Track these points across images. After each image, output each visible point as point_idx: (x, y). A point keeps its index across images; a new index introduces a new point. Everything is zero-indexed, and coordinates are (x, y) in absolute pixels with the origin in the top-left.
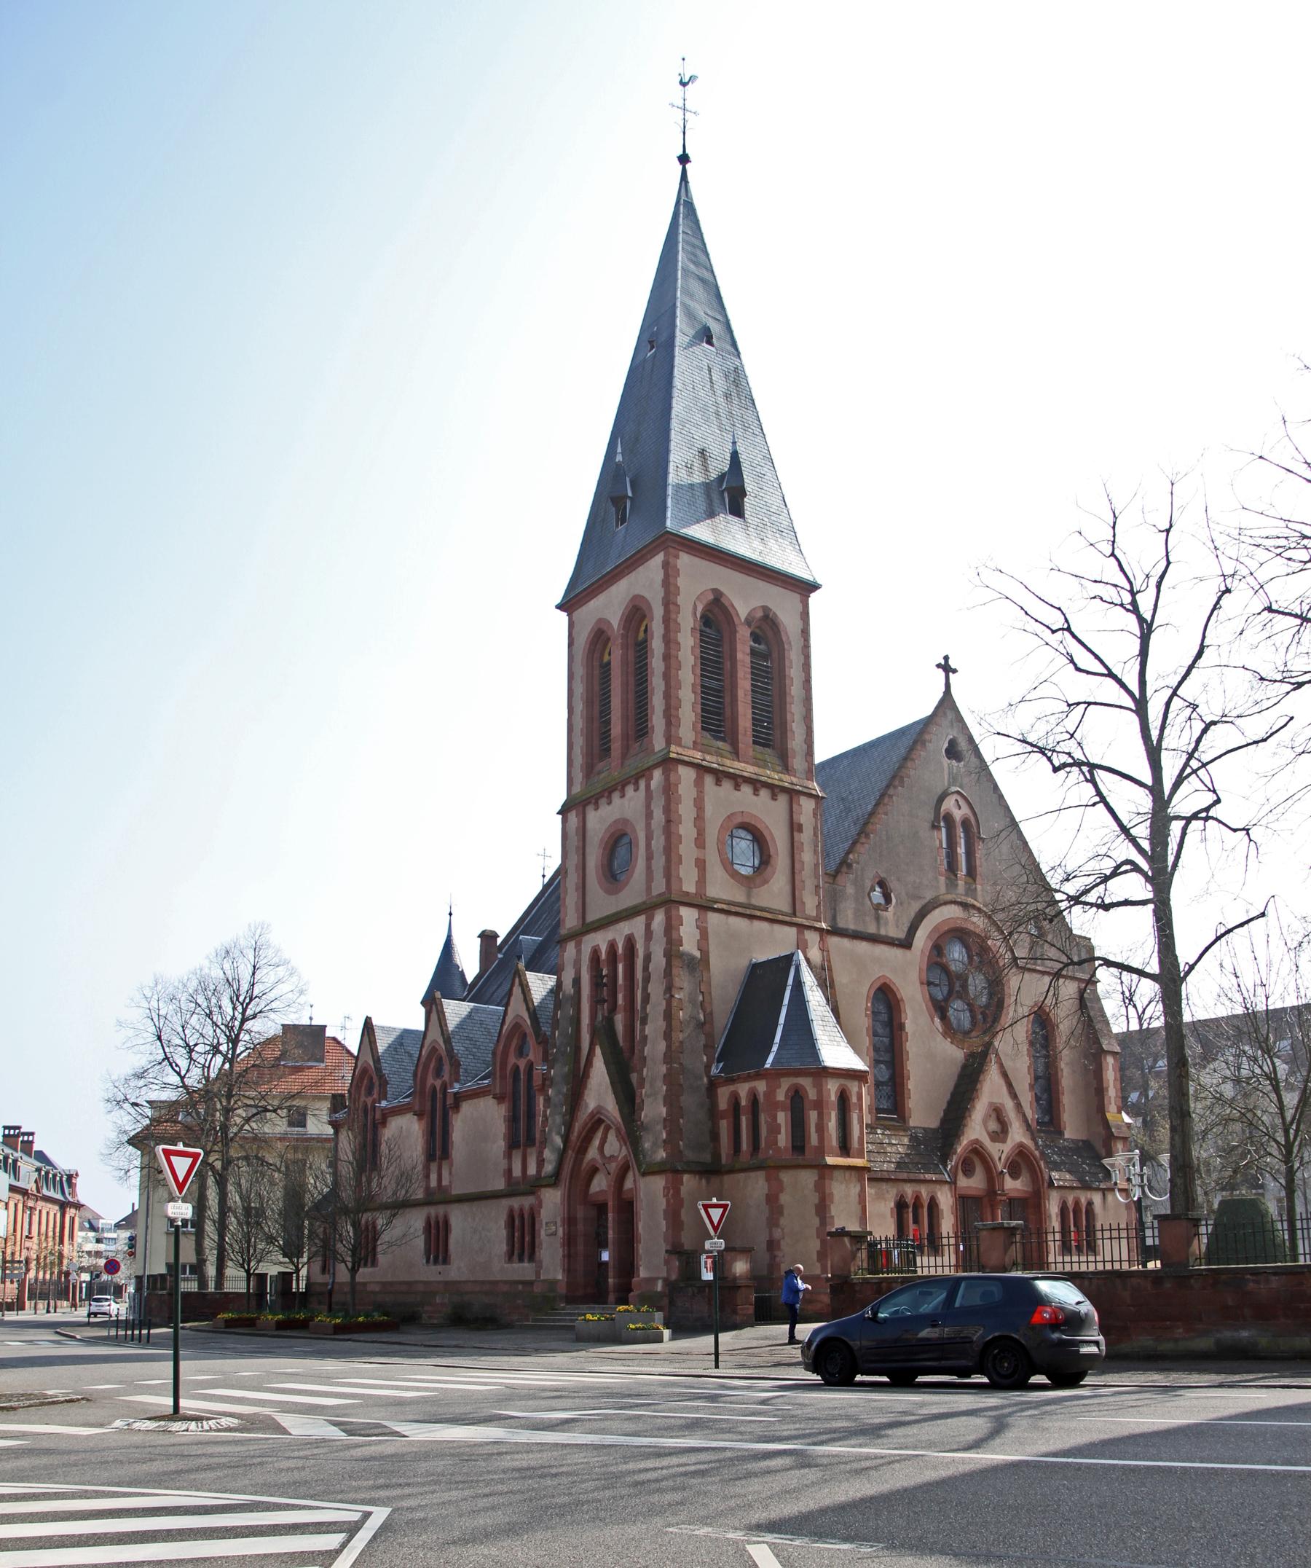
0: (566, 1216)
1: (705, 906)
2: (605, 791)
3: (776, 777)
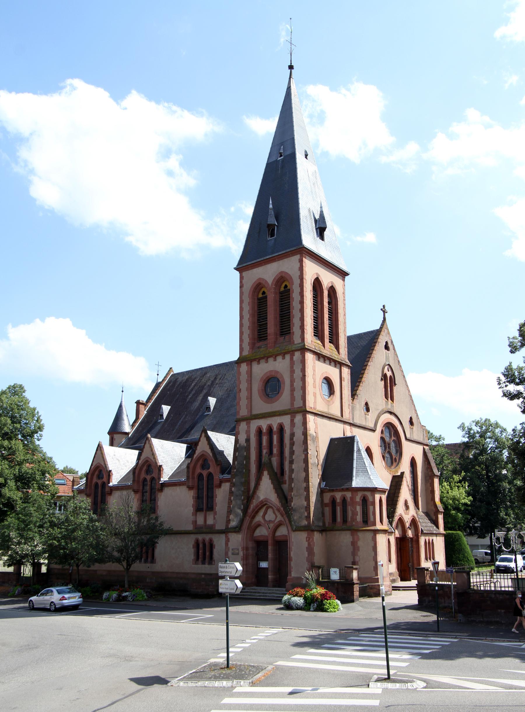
0: (245, 546)
3: (337, 357)
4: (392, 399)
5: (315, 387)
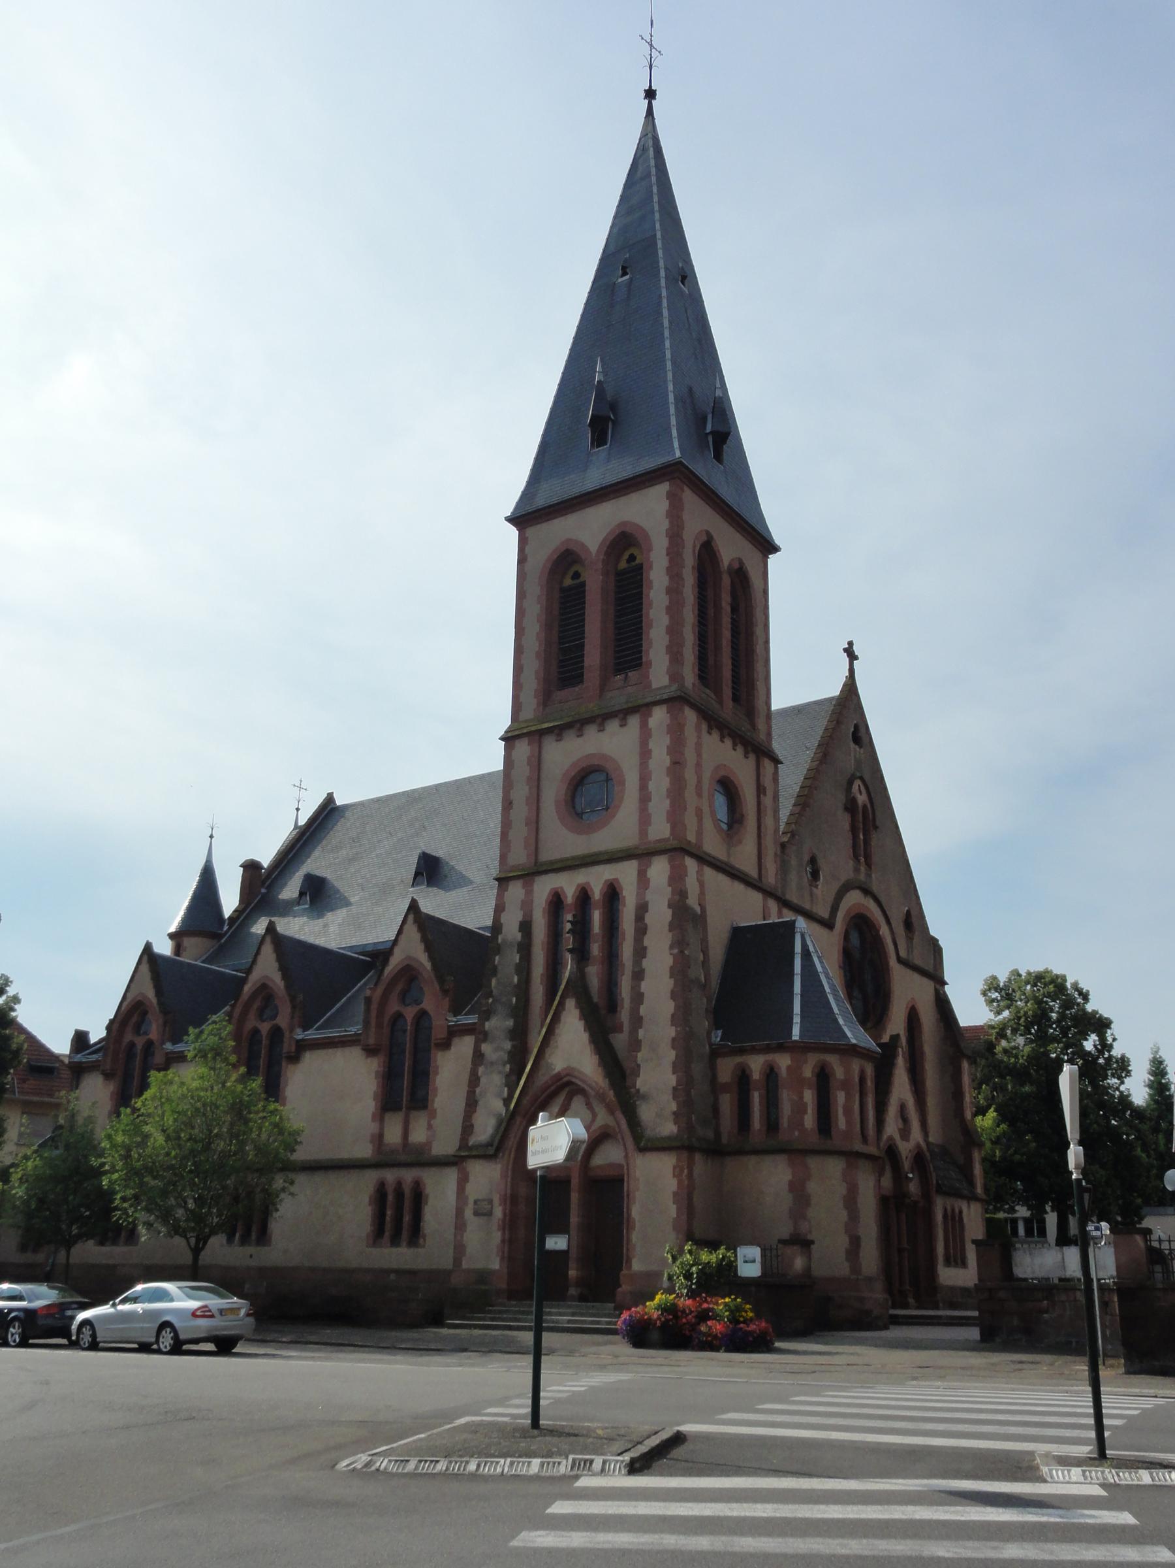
0: (509, 1191)
1: (704, 860)
2: (576, 722)
4: (869, 864)
5: (699, 794)
